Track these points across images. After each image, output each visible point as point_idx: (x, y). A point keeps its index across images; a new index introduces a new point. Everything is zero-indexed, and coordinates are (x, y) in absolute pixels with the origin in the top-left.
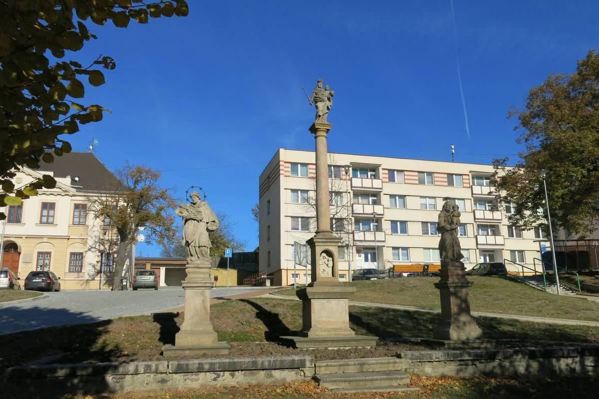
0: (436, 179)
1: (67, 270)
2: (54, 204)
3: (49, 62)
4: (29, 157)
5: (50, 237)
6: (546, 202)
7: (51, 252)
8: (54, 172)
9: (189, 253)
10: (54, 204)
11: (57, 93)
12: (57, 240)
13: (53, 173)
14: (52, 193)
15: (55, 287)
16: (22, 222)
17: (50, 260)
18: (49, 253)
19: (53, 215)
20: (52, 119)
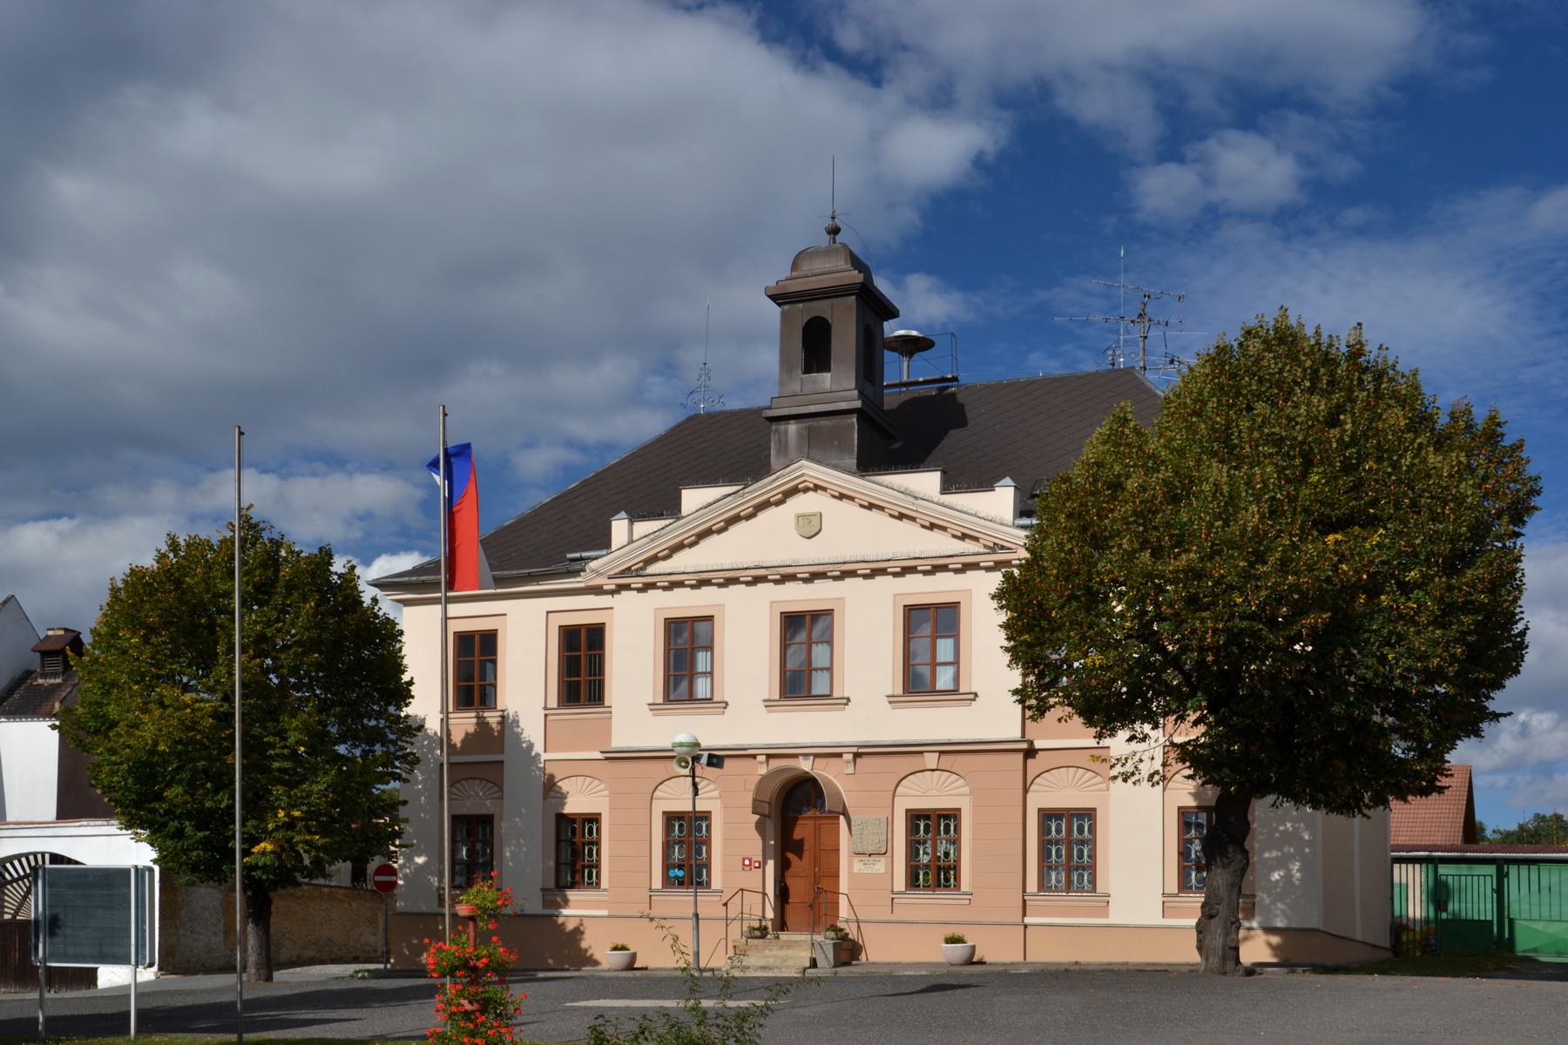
0: (16, 904)
1: (657, 883)
2: (954, 607)
3: (791, 892)
4: (420, 941)
5: (949, 750)
6: (468, 939)
7: (959, 810)
8: (944, 473)
9: (47, 886)
10: (954, 607)
11: (1272, 781)
12: (622, 762)
13: (1008, 478)
14: (705, 576)
15: (819, 684)
16: (274, 980)
17: (956, 842)
18: (952, 816)
19: (950, 658)
20: (1199, 597)
